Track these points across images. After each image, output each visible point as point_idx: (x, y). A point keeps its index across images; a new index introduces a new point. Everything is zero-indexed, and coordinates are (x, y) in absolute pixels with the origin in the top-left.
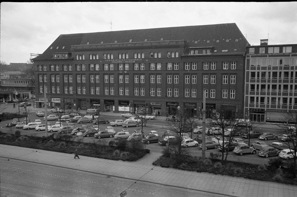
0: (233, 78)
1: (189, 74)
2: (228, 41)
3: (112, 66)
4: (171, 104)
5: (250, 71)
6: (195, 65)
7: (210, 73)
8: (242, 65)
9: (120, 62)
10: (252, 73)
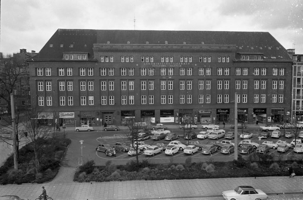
1: (85, 80)
3: (49, 71)
5: (297, 77)
6: (91, 70)
7: (260, 78)
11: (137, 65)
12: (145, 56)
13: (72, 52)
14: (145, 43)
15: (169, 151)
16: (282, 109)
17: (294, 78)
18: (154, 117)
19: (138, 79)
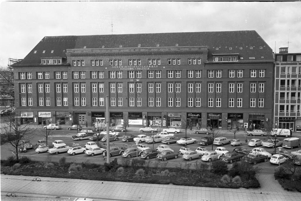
0: (262, 86)
1: (60, 83)
2: (252, 48)
4: (192, 115)
5: (280, 79)
7: (236, 81)
8: (272, 73)
9: (131, 69)
10: (281, 81)
11: (106, 68)
12: (197, 58)
13: (51, 57)
14: (119, 47)
15: (275, 160)
16: (262, 114)
17: (276, 79)
18: (123, 119)
19: (108, 82)
